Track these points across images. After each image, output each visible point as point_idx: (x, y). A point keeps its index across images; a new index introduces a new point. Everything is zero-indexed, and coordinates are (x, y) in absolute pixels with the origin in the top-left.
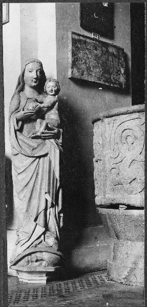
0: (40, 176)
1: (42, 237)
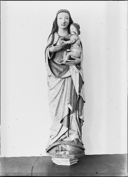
0: (65, 90)
1: (67, 134)
